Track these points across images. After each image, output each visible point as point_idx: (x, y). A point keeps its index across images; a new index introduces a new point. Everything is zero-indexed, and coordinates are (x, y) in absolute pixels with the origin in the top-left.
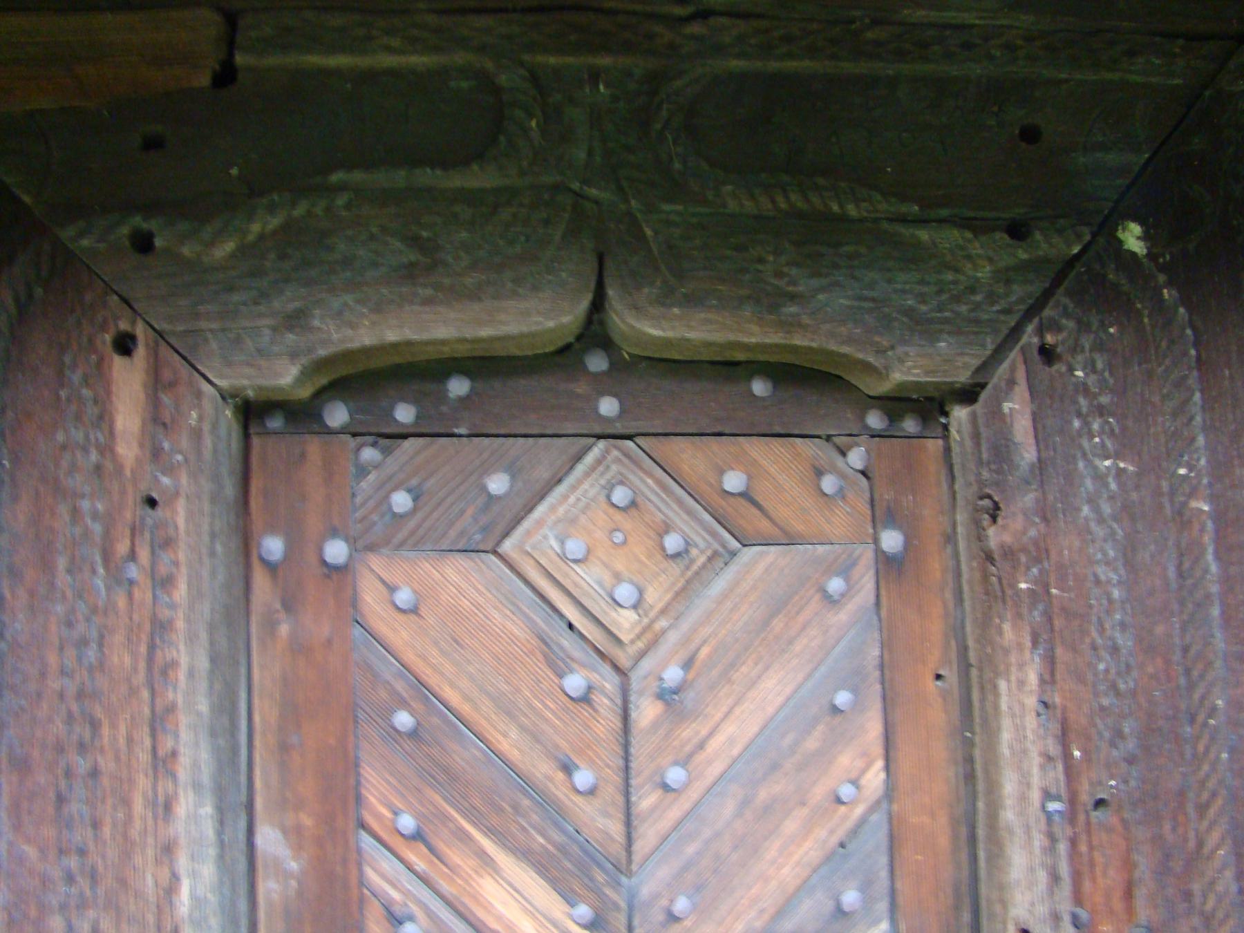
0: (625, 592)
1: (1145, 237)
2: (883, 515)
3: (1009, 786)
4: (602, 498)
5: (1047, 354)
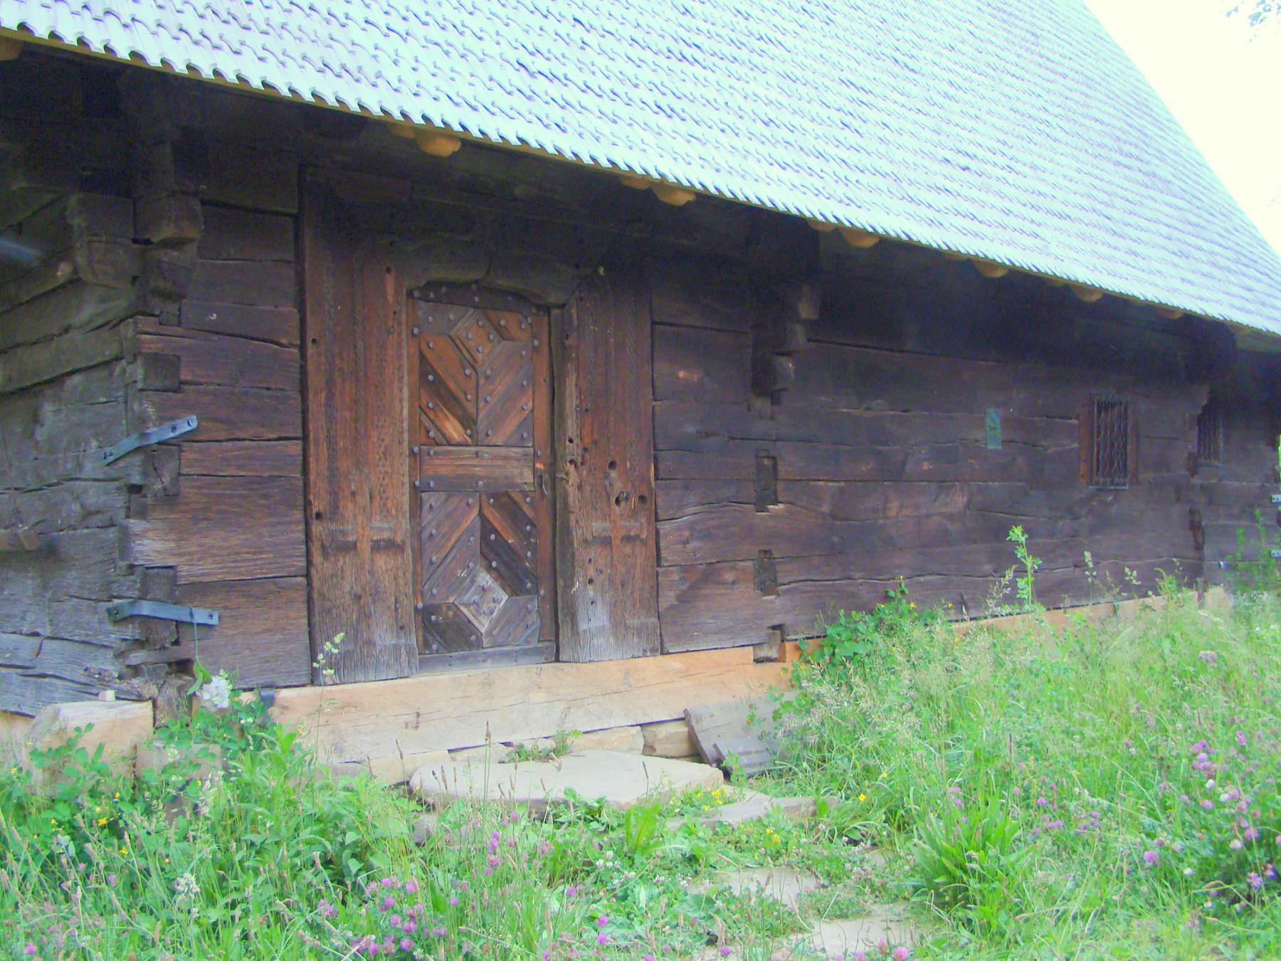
0: (480, 349)
1: (605, 271)
2: (534, 336)
3: (568, 404)
4: (475, 325)
5: (581, 299)
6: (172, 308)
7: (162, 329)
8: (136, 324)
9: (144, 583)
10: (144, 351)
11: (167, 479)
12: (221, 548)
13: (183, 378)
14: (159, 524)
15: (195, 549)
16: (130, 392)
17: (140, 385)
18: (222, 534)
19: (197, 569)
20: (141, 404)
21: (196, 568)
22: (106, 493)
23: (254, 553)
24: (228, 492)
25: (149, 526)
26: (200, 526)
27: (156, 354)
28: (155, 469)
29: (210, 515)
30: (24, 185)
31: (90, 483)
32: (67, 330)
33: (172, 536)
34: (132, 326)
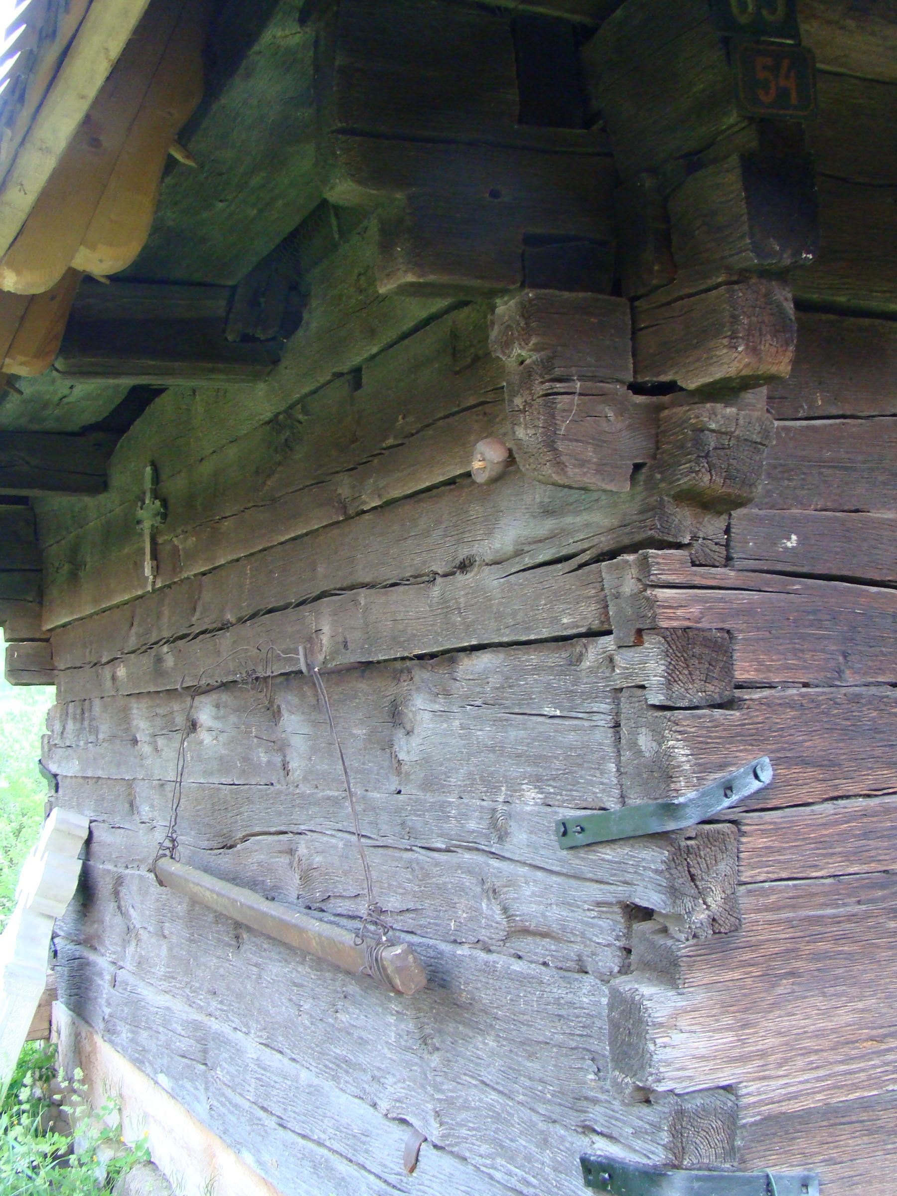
6: (713, 526)
7: (700, 575)
8: (644, 565)
9: (677, 1133)
10: (664, 624)
11: (716, 900)
12: (819, 1034)
13: (740, 675)
14: (700, 997)
15: (771, 1041)
16: (625, 707)
17: (656, 698)
18: (820, 1003)
19: (775, 1087)
20: (660, 739)
21: (774, 1084)
22: (569, 905)
23: (880, 1039)
24: (829, 911)
25: (682, 1003)
26: (780, 990)
27: (686, 629)
28: (693, 878)
29: (799, 964)
30: (410, 278)
31: (523, 870)
32: (464, 566)
33: (727, 1020)
34: (634, 571)
